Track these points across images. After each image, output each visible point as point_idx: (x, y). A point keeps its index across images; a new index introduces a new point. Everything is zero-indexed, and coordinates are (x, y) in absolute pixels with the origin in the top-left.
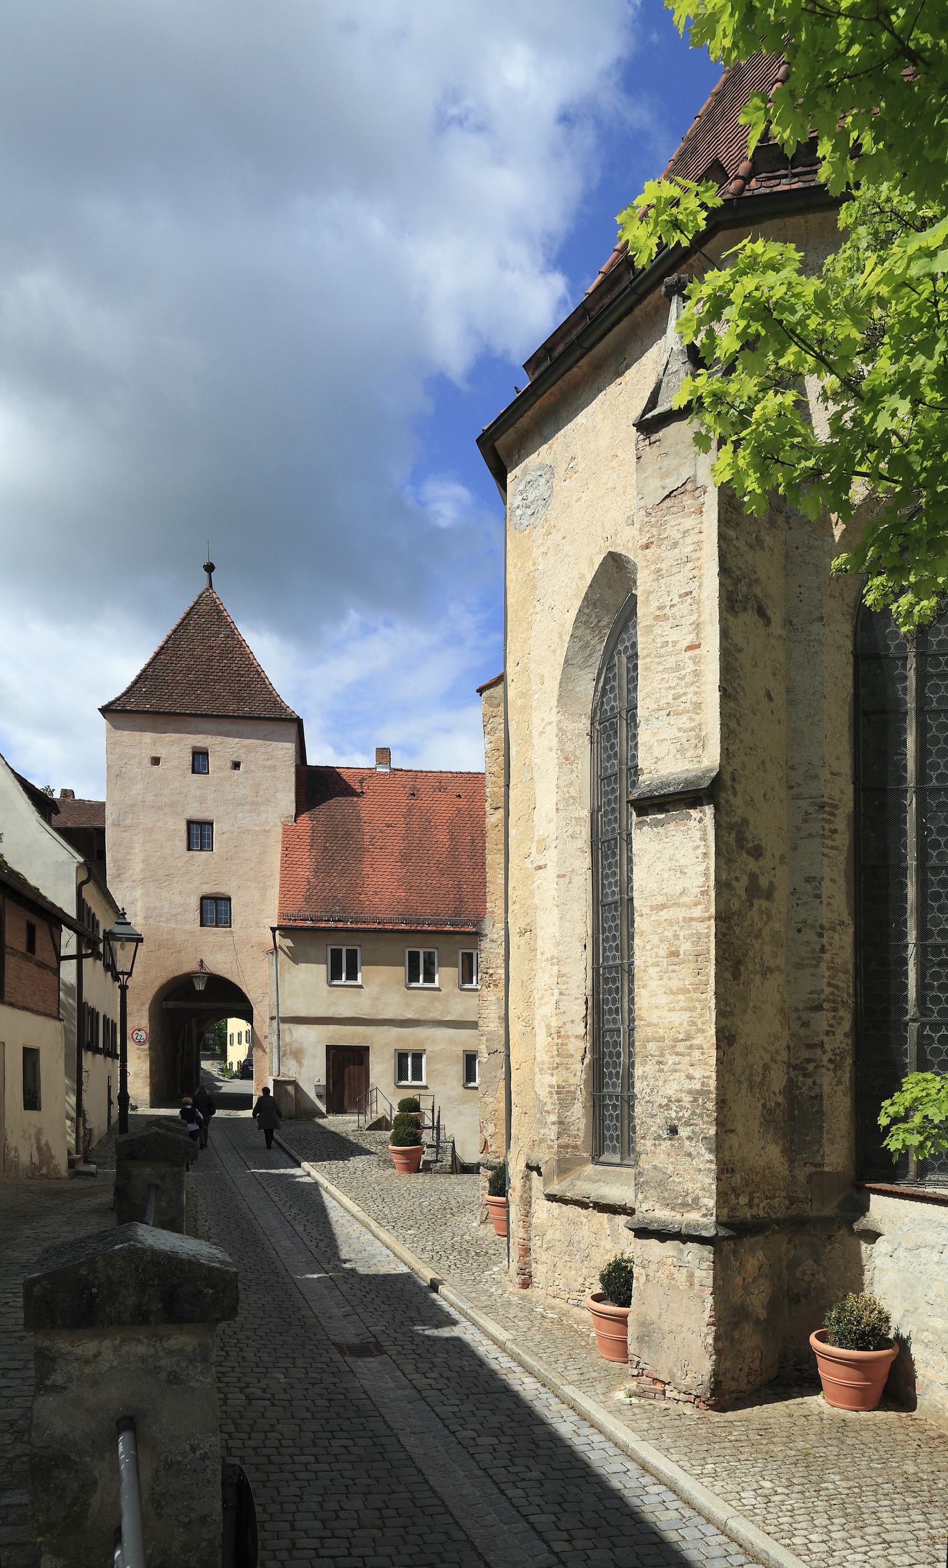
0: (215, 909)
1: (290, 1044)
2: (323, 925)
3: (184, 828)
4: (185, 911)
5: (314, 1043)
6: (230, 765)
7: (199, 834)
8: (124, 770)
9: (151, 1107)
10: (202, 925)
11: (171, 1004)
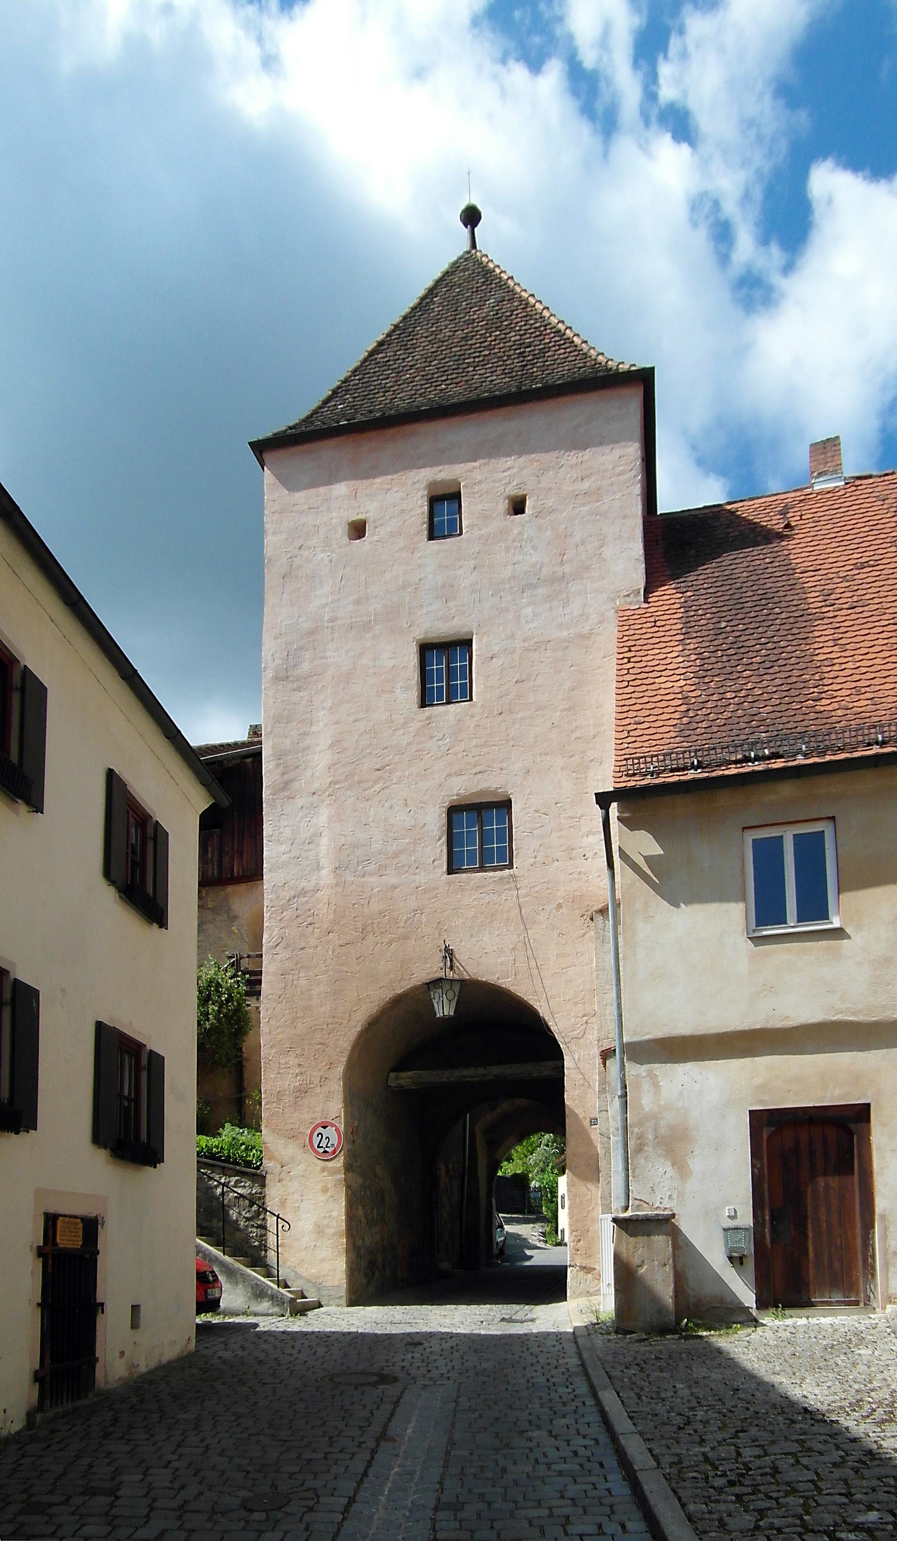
0: (478, 830)
1: (654, 1117)
2: (733, 771)
3: (413, 660)
4: (415, 842)
5: (717, 1104)
6: (503, 506)
7: (443, 668)
8: (297, 561)
9: (353, 1301)
10: (450, 871)
11: (406, 1078)
